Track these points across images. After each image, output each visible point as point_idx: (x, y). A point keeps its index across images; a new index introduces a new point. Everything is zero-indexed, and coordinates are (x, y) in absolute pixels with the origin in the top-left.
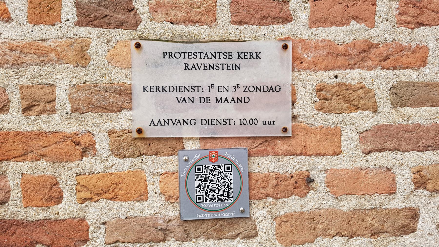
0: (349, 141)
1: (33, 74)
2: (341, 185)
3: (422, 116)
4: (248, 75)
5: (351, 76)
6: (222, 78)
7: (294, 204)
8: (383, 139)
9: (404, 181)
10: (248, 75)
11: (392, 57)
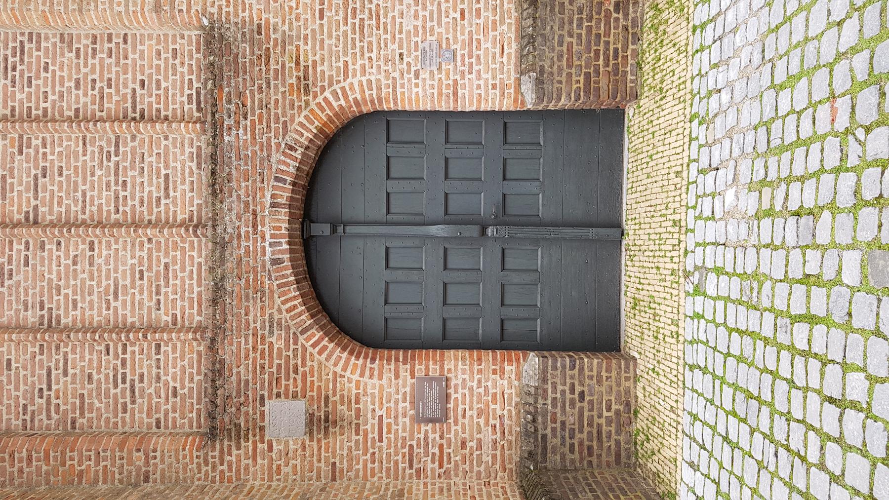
0: (440, 30)
1: (428, 88)
2: (448, 32)
3: (139, 2)
4: (428, 49)
5: (428, 30)
6: (428, 54)
7: (451, 41)
8: (439, 24)
9: (447, 20)
10: (428, 49)
11: (425, 22)
